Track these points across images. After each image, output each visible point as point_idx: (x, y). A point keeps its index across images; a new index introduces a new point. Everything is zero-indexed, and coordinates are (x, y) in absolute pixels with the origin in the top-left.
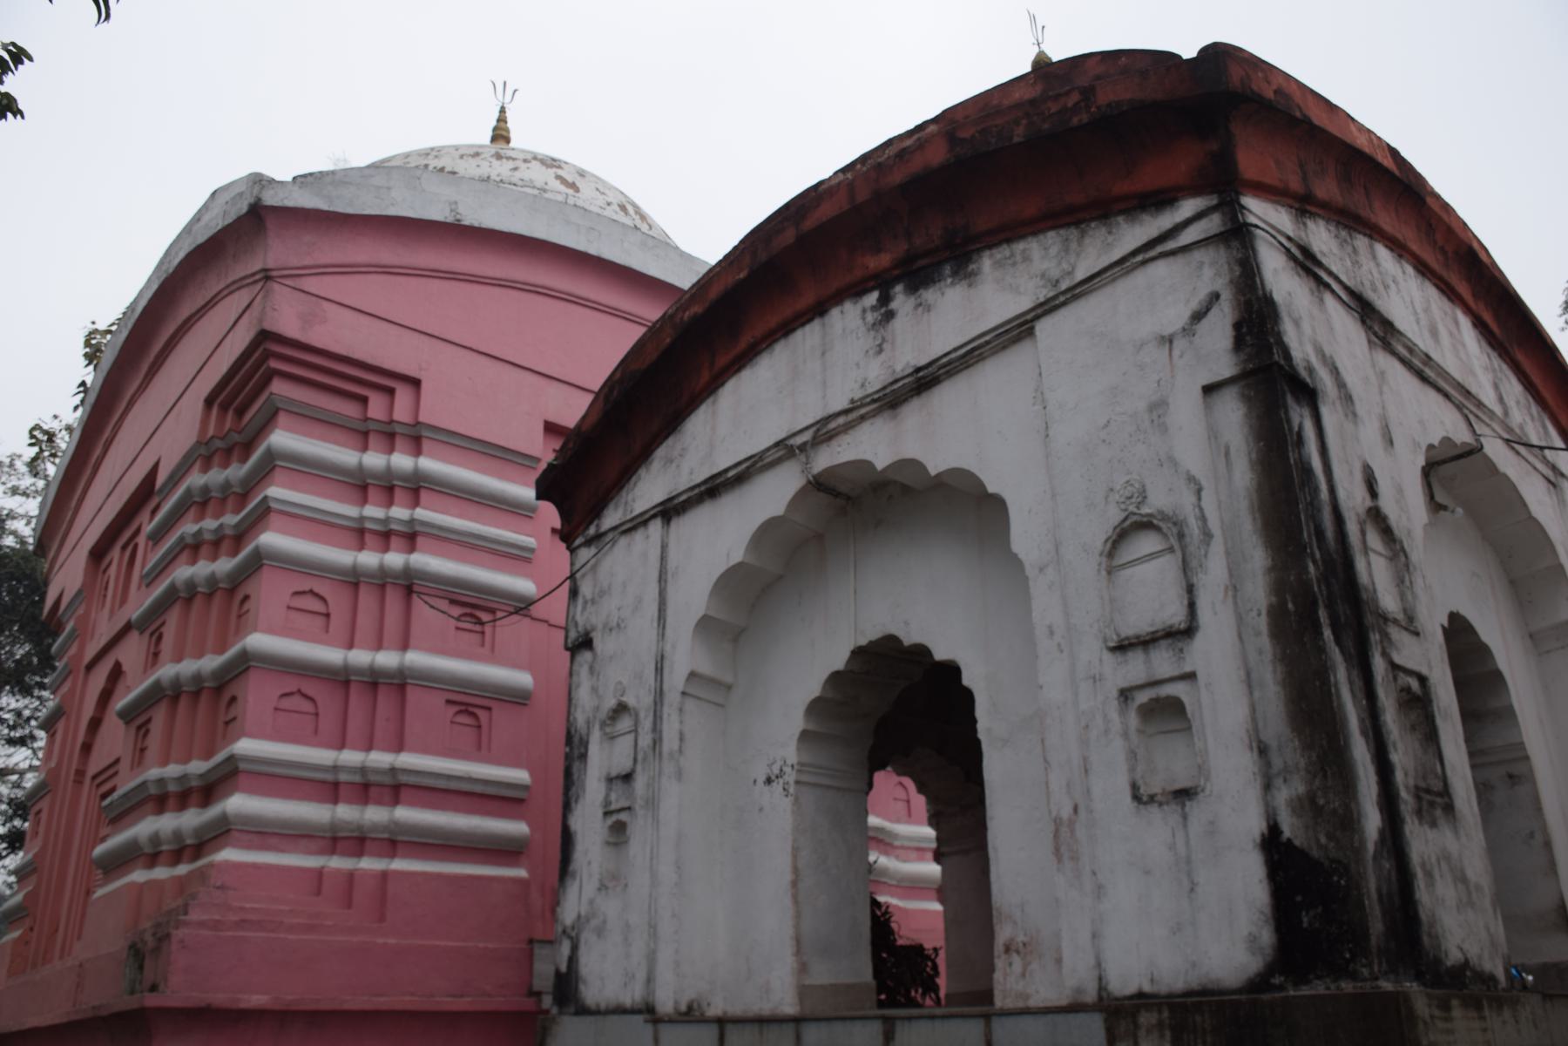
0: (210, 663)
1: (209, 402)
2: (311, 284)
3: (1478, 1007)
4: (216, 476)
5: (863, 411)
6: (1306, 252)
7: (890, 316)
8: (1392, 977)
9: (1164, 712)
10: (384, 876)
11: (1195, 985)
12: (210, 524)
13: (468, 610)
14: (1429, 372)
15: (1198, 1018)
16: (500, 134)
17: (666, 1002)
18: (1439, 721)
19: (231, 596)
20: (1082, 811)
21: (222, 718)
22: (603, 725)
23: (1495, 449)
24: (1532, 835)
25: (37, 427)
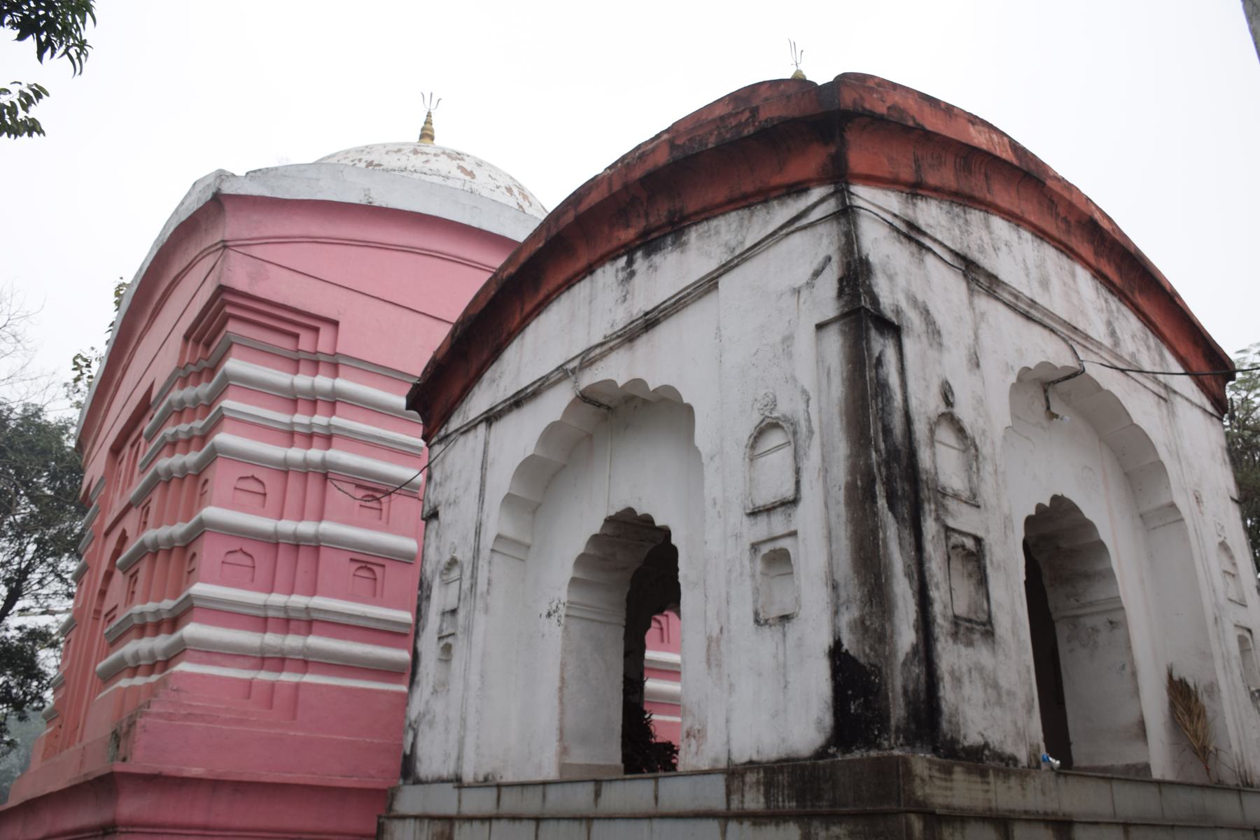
0: (180, 528)
1: (187, 337)
2: (257, 251)
3: (983, 773)
4: (189, 392)
5: (612, 344)
6: (911, 225)
7: (632, 274)
8: (908, 749)
9: (778, 560)
10: (297, 686)
11: (783, 756)
12: (184, 427)
13: (370, 493)
14: (1033, 312)
15: (781, 777)
16: (427, 134)
17: (468, 777)
18: (989, 570)
19: (196, 478)
20: (725, 630)
21: (187, 569)
22: (442, 574)
23: (1093, 370)
24: (1123, 667)
25: (79, 356)
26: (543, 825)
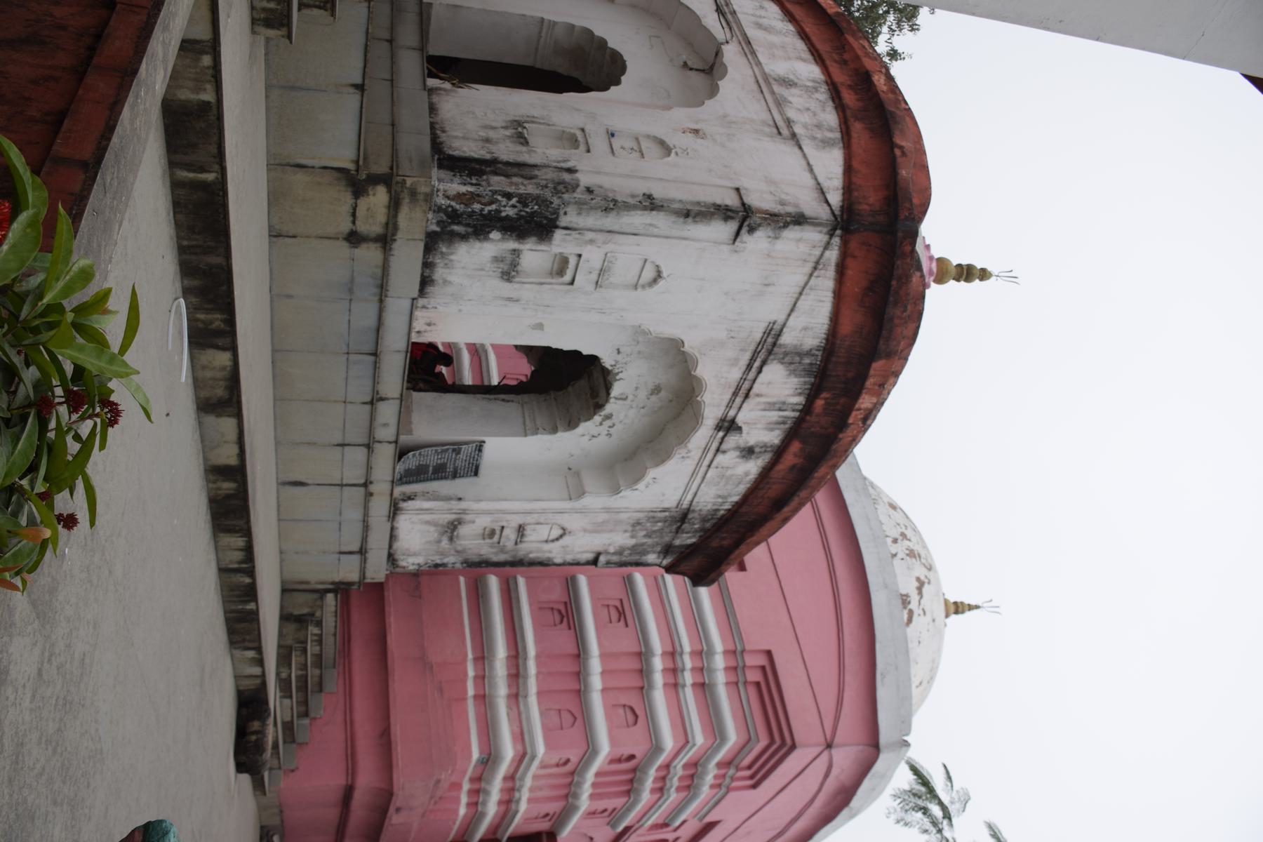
16: (959, 608)
26: (365, 450)
